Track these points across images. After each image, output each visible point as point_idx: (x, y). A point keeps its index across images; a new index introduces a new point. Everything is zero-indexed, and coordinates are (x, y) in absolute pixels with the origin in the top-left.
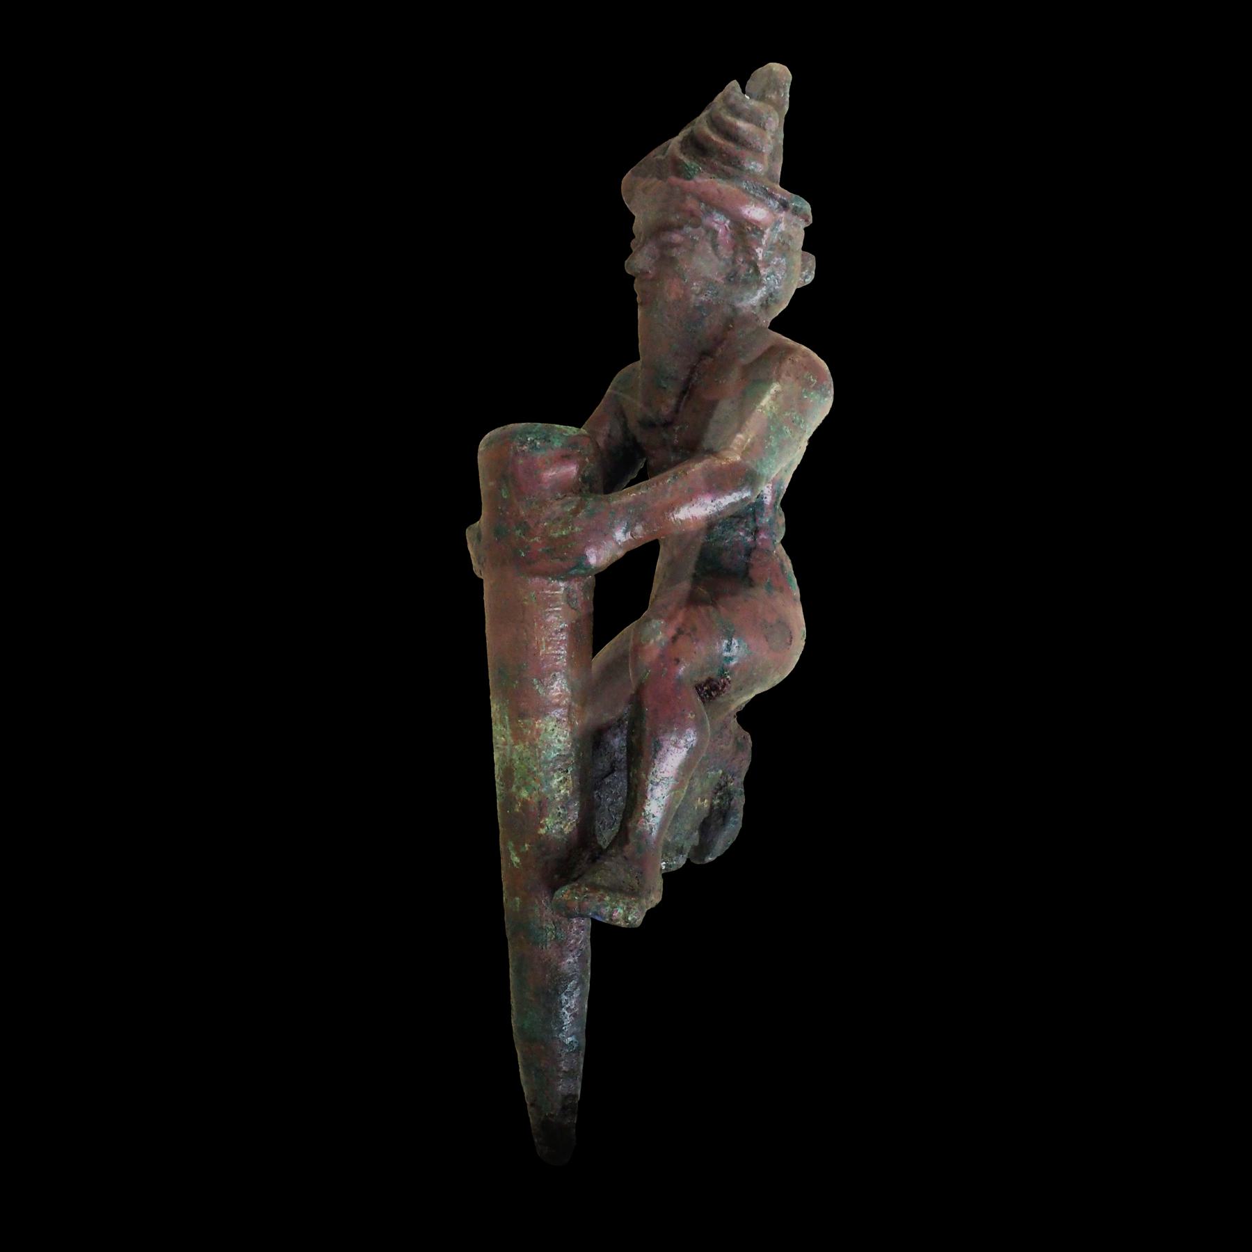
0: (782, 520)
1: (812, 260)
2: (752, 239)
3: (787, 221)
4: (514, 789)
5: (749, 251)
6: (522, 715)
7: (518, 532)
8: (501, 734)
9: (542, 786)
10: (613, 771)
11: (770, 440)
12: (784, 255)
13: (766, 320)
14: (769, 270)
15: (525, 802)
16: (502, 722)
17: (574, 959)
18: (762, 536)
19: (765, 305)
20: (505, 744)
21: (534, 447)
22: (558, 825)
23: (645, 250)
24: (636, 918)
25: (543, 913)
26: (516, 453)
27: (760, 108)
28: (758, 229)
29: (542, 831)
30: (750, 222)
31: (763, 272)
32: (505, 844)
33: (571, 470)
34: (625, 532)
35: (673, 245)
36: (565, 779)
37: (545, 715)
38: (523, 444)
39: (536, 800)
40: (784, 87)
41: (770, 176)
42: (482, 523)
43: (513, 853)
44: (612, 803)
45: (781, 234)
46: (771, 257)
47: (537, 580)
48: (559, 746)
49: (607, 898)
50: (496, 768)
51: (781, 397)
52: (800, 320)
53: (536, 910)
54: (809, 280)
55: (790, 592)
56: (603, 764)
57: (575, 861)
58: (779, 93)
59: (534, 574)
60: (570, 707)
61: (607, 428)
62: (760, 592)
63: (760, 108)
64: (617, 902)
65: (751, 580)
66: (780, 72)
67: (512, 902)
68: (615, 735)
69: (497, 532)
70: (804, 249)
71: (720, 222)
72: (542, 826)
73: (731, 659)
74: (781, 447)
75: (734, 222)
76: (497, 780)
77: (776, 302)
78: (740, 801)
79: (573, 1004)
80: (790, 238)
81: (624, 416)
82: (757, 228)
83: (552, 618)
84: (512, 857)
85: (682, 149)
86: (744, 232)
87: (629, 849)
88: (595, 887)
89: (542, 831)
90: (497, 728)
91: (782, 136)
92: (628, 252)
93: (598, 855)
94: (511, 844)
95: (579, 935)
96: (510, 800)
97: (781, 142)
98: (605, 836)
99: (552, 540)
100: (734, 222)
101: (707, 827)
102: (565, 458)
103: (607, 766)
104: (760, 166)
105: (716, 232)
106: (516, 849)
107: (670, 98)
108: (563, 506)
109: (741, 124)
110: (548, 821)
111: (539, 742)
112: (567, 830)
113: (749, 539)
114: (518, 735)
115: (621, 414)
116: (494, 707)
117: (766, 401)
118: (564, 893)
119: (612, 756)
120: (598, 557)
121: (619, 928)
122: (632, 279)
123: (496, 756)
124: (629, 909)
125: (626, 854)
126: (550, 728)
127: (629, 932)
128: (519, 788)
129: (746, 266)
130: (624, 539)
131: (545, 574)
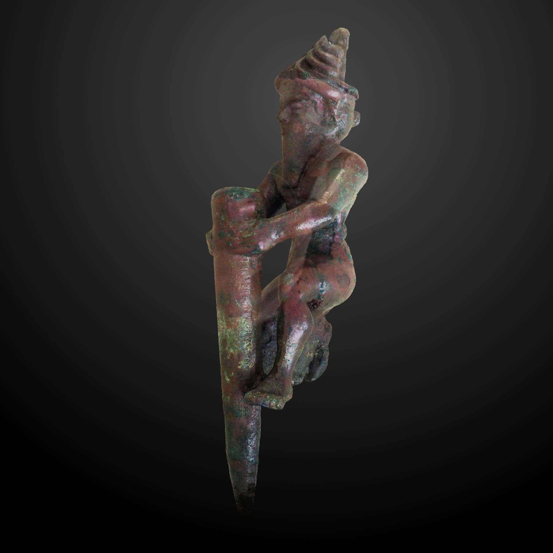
0: (345, 230)
1: (359, 116)
2: (332, 106)
3: (348, 98)
4: (227, 348)
5: (331, 111)
6: (231, 316)
7: (229, 235)
8: (221, 324)
9: (239, 347)
10: (271, 340)
11: (340, 194)
12: (346, 113)
14: (339, 119)
15: (232, 354)
16: (222, 319)
17: (253, 423)
18: (337, 237)
20: (223, 329)
21: (236, 198)
22: (247, 364)
25: (240, 403)
26: (228, 200)
28: (335, 101)
29: (240, 367)
30: (331, 98)
31: (337, 120)
32: (223, 373)
33: (252, 208)
34: (276, 235)
35: (297, 108)
36: (250, 344)
37: (241, 316)
38: (231, 196)
39: (237, 353)
42: (213, 231)
43: (227, 377)
44: (270, 355)
45: (345, 103)
46: (341, 113)
47: (237, 256)
48: (247, 330)
49: (268, 397)
50: (219, 339)
51: (345, 175)
53: (237, 402)
54: (357, 124)
55: (349, 261)
56: (266, 337)
57: (254, 380)
58: (344, 41)
59: (236, 253)
60: (252, 312)
61: (268, 189)
62: (336, 261)
64: (273, 398)
65: (332, 256)
67: (226, 399)
68: (272, 325)
69: (220, 235)
71: (318, 98)
72: (239, 365)
73: (323, 291)
74: (345, 197)
78: (327, 354)
79: (253, 444)
80: (349, 105)
81: (276, 184)
82: (334, 101)
83: (244, 273)
85: (301, 66)
86: (329, 103)
87: (278, 375)
88: (263, 392)
89: (240, 367)
90: (219, 322)
91: (346, 60)
93: (264, 378)
94: (226, 373)
95: (256, 413)
96: (225, 353)
98: (267, 369)
99: (244, 238)
101: (313, 365)
102: (249, 202)
103: (268, 338)
104: (336, 73)
105: (316, 103)
106: (228, 375)
108: (249, 223)
109: (327, 55)
110: (242, 363)
112: (250, 367)
113: (331, 238)
114: (229, 325)
116: (218, 312)
117: (338, 177)
118: (249, 395)
119: (271, 334)
121: (273, 410)
124: (278, 401)
125: (277, 377)
126: (243, 322)
127: (278, 411)
128: (229, 348)
129: (330, 117)
130: (275, 238)
131: (241, 254)
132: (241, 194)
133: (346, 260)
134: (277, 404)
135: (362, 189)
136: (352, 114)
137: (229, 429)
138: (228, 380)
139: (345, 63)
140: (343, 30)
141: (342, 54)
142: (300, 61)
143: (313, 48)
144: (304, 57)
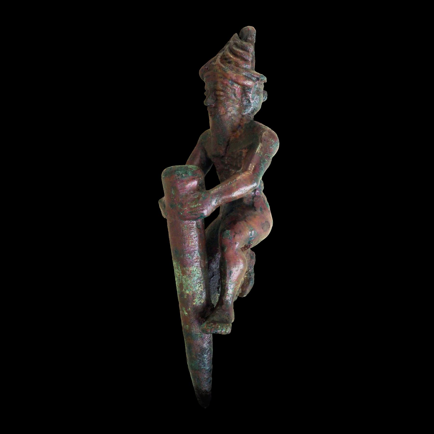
0: (263, 185)
1: (266, 94)
2: (248, 92)
3: (259, 83)
4: (184, 290)
5: (246, 95)
6: (185, 267)
7: (179, 206)
8: (177, 272)
9: (193, 289)
10: (213, 276)
11: (261, 165)
12: (258, 95)
13: (252, 117)
14: (253, 101)
15: (188, 295)
16: (178, 268)
17: (206, 343)
18: (257, 191)
19: (253, 112)
20: (179, 275)
21: (182, 177)
22: (199, 301)
23: (211, 97)
25: (196, 329)
26: (176, 180)
27: (246, 43)
28: (249, 88)
29: (194, 304)
30: (247, 86)
31: (251, 102)
32: (182, 308)
33: (195, 183)
34: (216, 203)
35: (220, 96)
36: (201, 286)
37: (193, 266)
38: (178, 175)
39: (192, 293)
40: (254, 35)
41: (252, 68)
42: (164, 199)
43: (185, 311)
44: (214, 286)
45: (257, 88)
46: (254, 96)
47: (187, 221)
48: (198, 275)
49: (219, 327)
50: (176, 283)
51: (263, 149)
52: (264, 115)
53: (194, 329)
54: (266, 99)
55: (267, 209)
56: (210, 274)
57: (207, 312)
58: (252, 37)
59: (185, 220)
60: (200, 262)
61: (200, 154)
62: (259, 211)
63: (246, 43)
64: (223, 327)
65: (255, 207)
66: (252, 29)
67: (185, 327)
68: (213, 264)
69: (172, 206)
70: (264, 89)
71: (237, 88)
72: (194, 302)
73: (252, 238)
75: (241, 88)
78: (253, 275)
80: (260, 89)
81: (205, 151)
82: (249, 88)
83: (193, 233)
84: (184, 313)
85: (221, 61)
86: (245, 90)
87: (224, 306)
88: (215, 322)
89: (194, 304)
90: (176, 271)
91: (254, 53)
92: (204, 97)
93: (213, 309)
94: (184, 309)
96: (182, 294)
97: (254, 55)
99: (191, 209)
100: (241, 88)
101: (243, 287)
102: (193, 179)
103: (212, 274)
104: (249, 66)
105: (235, 90)
106: (186, 310)
107: (215, 43)
108: (194, 196)
109: (238, 50)
110: (196, 300)
112: (202, 302)
113: (253, 193)
114: (184, 273)
115: (204, 150)
116: (174, 263)
117: (258, 150)
118: (204, 325)
119: (216, 276)
120: (206, 212)
121: (224, 335)
122: (206, 107)
123: (176, 279)
124: (226, 329)
125: (223, 308)
126: (194, 270)
127: (227, 335)
128: (185, 290)
129: (246, 100)
130: (215, 205)
131: (189, 219)
132: (186, 173)
135: (212, 58)
136: (262, 95)
137: (189, 348)
138: (186, 313)
141: (252, 49)
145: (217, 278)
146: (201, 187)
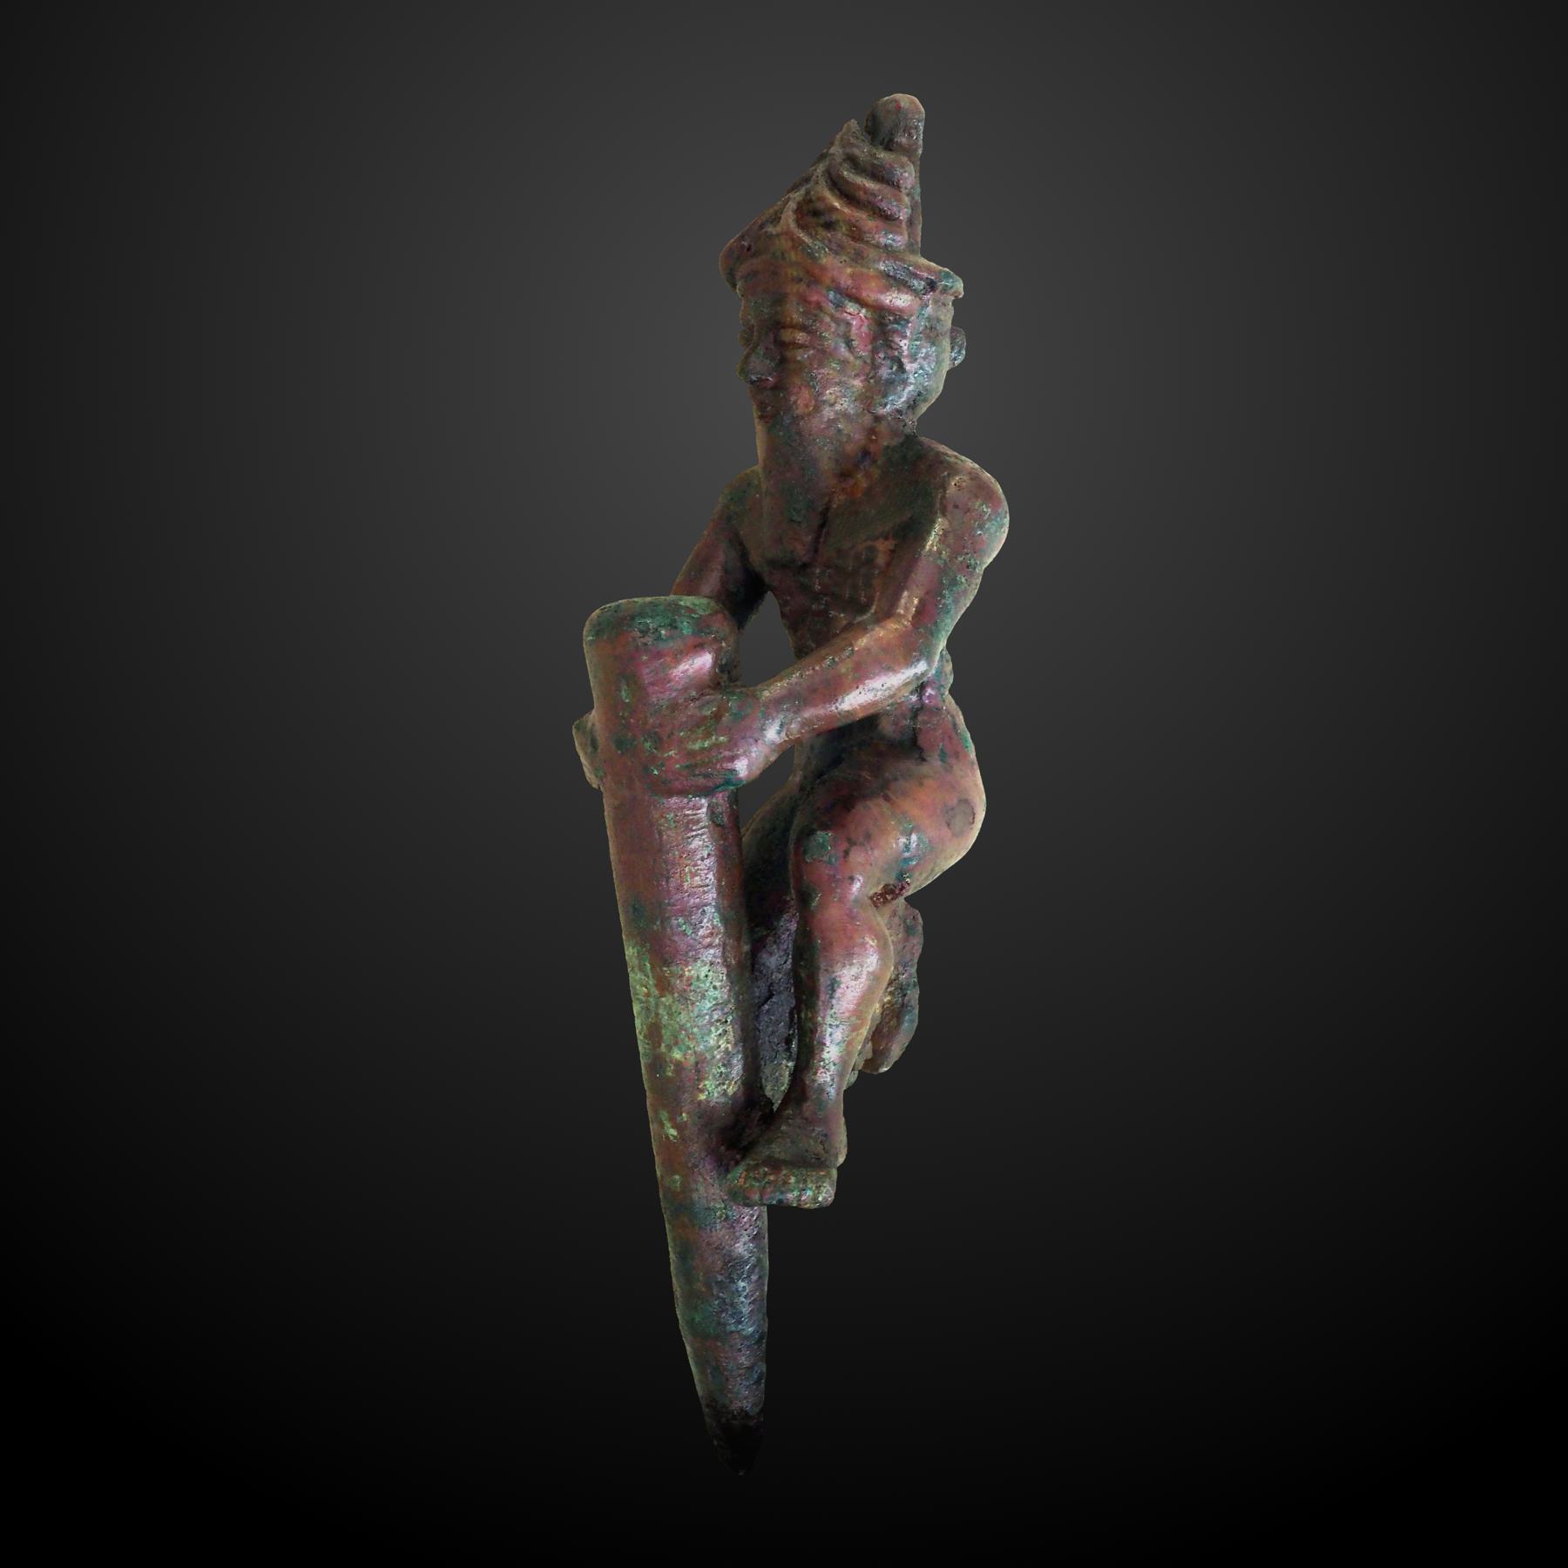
0: (949, 667)
1: (961, 339)
2: (895, 331)
3: (936, 302)
4: (663, 1049)
5: (889, 345)
6: (667, 963)
7: (648, 745)
8: (640, 982)
9: (698, 1044)
10: (771, 996)
11: (943, 597)
12: (933, 344)
14: (915, 365)
15: (678, 1064)
16: (642, 969)
17: (744, 1237)
18: (929, 691)
20: (648, 995)
21: (659, 638)
22: (719, 1087)
24: (826, 1194)
25: (708, 1190)
26: (637, 649)
28: (901, 318)
29: (702, 1097)
30: (891, 310)
31: (908, 367)
32: (656, 1112)
34: (779, 733)
35: (796, 345)
36: (725, 1032)
37: (696, 960)
38: (644, 633)
39: (692, 1060)
42: (594, 718)
43: (668, 1125)
44: (773, 1032)
45: (929, 319)
46: (919, 348)
47: (674, 800)
48: (717, 994)
49: (793, 1180)
50: (638, 1023)
51: (951, 540)
53: (702, 1189)
55: (966, 756)
56: (760, 990)
58: (910, 135)
59: (670, 793)
60: (724, 945)
62: (935, 762)
64: (805, 1181)
65: (921, 750)
68: (771, 954)
69: (620, 744)
71: (857, 317)
72: (702, 1091)
73: (910, 859)
76: (640, 1037)
77: (925, 400)
78: (914, 995)
79: (747, 1292)
80: (939, 320)
81: (741, 544)
82: (900, 317)
83: (696, 843)
85: (797, 221)
86: (885, 324)
87: (808, 1107)
88: (775, 1165)
89: (702, 1097)
90: (635, 977)
93: (770, 1118)
94: (664, 1115)
95: (752, 1218)
96: (658, 1063)
98: (777, 1082)
99: (692, 754)
101: (879, 1035)
102: (698, 647)
103: (764, 990)
104: (898, 238)
105: (848, 324)
106: (672, 1119)
108: (700, 708)
109: (860, 180)
110: (709, 1084)
111: (695, 1020)
112: (731, 1091)
113: (914, 698)
114: (664, 986)
116: (630, 952)
117: (932, 542)
118: (738, 1175)
119: (781, 998)
124: (818, 1188)
125: (807, 1114)
126: (702, 975)
127: (822, 1211)
128: (669, 1048)
129: (888, 362)
130: (778, 740)
131: (683, 793)
132: (673, 626)
133: (958, 754)
134: (820, 1192)
136: (946, 343)
138: (673, 1132)
139: (918, 198)
140: (906, 100)
141: (909, 176)
142: (792, 205)
143: (823, 157)
144: (802, 191)
145: (783, 1003)
146: (725, 677)
